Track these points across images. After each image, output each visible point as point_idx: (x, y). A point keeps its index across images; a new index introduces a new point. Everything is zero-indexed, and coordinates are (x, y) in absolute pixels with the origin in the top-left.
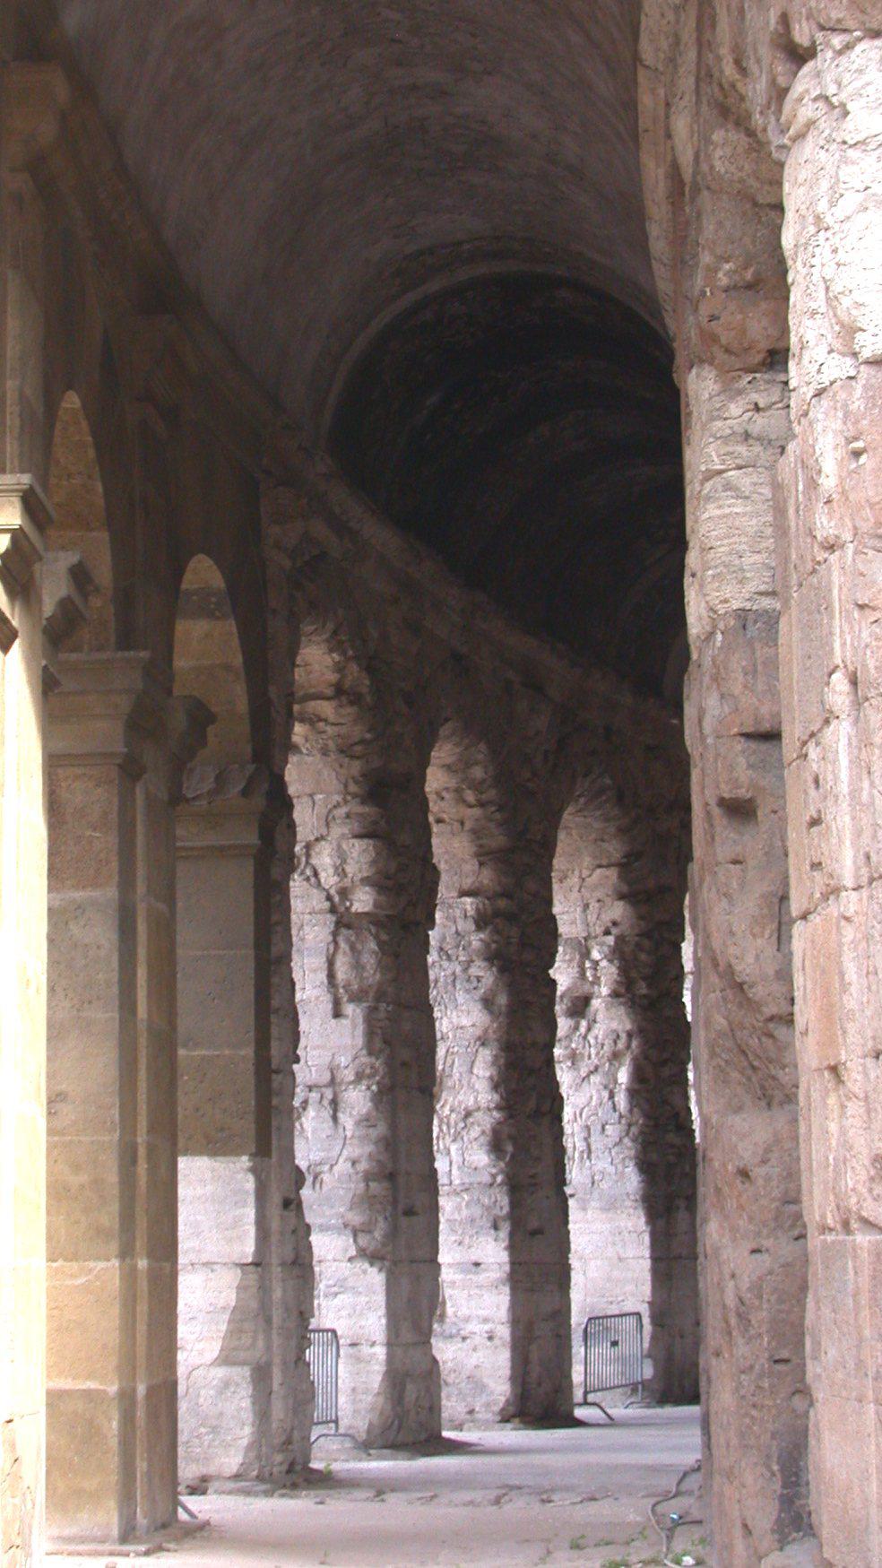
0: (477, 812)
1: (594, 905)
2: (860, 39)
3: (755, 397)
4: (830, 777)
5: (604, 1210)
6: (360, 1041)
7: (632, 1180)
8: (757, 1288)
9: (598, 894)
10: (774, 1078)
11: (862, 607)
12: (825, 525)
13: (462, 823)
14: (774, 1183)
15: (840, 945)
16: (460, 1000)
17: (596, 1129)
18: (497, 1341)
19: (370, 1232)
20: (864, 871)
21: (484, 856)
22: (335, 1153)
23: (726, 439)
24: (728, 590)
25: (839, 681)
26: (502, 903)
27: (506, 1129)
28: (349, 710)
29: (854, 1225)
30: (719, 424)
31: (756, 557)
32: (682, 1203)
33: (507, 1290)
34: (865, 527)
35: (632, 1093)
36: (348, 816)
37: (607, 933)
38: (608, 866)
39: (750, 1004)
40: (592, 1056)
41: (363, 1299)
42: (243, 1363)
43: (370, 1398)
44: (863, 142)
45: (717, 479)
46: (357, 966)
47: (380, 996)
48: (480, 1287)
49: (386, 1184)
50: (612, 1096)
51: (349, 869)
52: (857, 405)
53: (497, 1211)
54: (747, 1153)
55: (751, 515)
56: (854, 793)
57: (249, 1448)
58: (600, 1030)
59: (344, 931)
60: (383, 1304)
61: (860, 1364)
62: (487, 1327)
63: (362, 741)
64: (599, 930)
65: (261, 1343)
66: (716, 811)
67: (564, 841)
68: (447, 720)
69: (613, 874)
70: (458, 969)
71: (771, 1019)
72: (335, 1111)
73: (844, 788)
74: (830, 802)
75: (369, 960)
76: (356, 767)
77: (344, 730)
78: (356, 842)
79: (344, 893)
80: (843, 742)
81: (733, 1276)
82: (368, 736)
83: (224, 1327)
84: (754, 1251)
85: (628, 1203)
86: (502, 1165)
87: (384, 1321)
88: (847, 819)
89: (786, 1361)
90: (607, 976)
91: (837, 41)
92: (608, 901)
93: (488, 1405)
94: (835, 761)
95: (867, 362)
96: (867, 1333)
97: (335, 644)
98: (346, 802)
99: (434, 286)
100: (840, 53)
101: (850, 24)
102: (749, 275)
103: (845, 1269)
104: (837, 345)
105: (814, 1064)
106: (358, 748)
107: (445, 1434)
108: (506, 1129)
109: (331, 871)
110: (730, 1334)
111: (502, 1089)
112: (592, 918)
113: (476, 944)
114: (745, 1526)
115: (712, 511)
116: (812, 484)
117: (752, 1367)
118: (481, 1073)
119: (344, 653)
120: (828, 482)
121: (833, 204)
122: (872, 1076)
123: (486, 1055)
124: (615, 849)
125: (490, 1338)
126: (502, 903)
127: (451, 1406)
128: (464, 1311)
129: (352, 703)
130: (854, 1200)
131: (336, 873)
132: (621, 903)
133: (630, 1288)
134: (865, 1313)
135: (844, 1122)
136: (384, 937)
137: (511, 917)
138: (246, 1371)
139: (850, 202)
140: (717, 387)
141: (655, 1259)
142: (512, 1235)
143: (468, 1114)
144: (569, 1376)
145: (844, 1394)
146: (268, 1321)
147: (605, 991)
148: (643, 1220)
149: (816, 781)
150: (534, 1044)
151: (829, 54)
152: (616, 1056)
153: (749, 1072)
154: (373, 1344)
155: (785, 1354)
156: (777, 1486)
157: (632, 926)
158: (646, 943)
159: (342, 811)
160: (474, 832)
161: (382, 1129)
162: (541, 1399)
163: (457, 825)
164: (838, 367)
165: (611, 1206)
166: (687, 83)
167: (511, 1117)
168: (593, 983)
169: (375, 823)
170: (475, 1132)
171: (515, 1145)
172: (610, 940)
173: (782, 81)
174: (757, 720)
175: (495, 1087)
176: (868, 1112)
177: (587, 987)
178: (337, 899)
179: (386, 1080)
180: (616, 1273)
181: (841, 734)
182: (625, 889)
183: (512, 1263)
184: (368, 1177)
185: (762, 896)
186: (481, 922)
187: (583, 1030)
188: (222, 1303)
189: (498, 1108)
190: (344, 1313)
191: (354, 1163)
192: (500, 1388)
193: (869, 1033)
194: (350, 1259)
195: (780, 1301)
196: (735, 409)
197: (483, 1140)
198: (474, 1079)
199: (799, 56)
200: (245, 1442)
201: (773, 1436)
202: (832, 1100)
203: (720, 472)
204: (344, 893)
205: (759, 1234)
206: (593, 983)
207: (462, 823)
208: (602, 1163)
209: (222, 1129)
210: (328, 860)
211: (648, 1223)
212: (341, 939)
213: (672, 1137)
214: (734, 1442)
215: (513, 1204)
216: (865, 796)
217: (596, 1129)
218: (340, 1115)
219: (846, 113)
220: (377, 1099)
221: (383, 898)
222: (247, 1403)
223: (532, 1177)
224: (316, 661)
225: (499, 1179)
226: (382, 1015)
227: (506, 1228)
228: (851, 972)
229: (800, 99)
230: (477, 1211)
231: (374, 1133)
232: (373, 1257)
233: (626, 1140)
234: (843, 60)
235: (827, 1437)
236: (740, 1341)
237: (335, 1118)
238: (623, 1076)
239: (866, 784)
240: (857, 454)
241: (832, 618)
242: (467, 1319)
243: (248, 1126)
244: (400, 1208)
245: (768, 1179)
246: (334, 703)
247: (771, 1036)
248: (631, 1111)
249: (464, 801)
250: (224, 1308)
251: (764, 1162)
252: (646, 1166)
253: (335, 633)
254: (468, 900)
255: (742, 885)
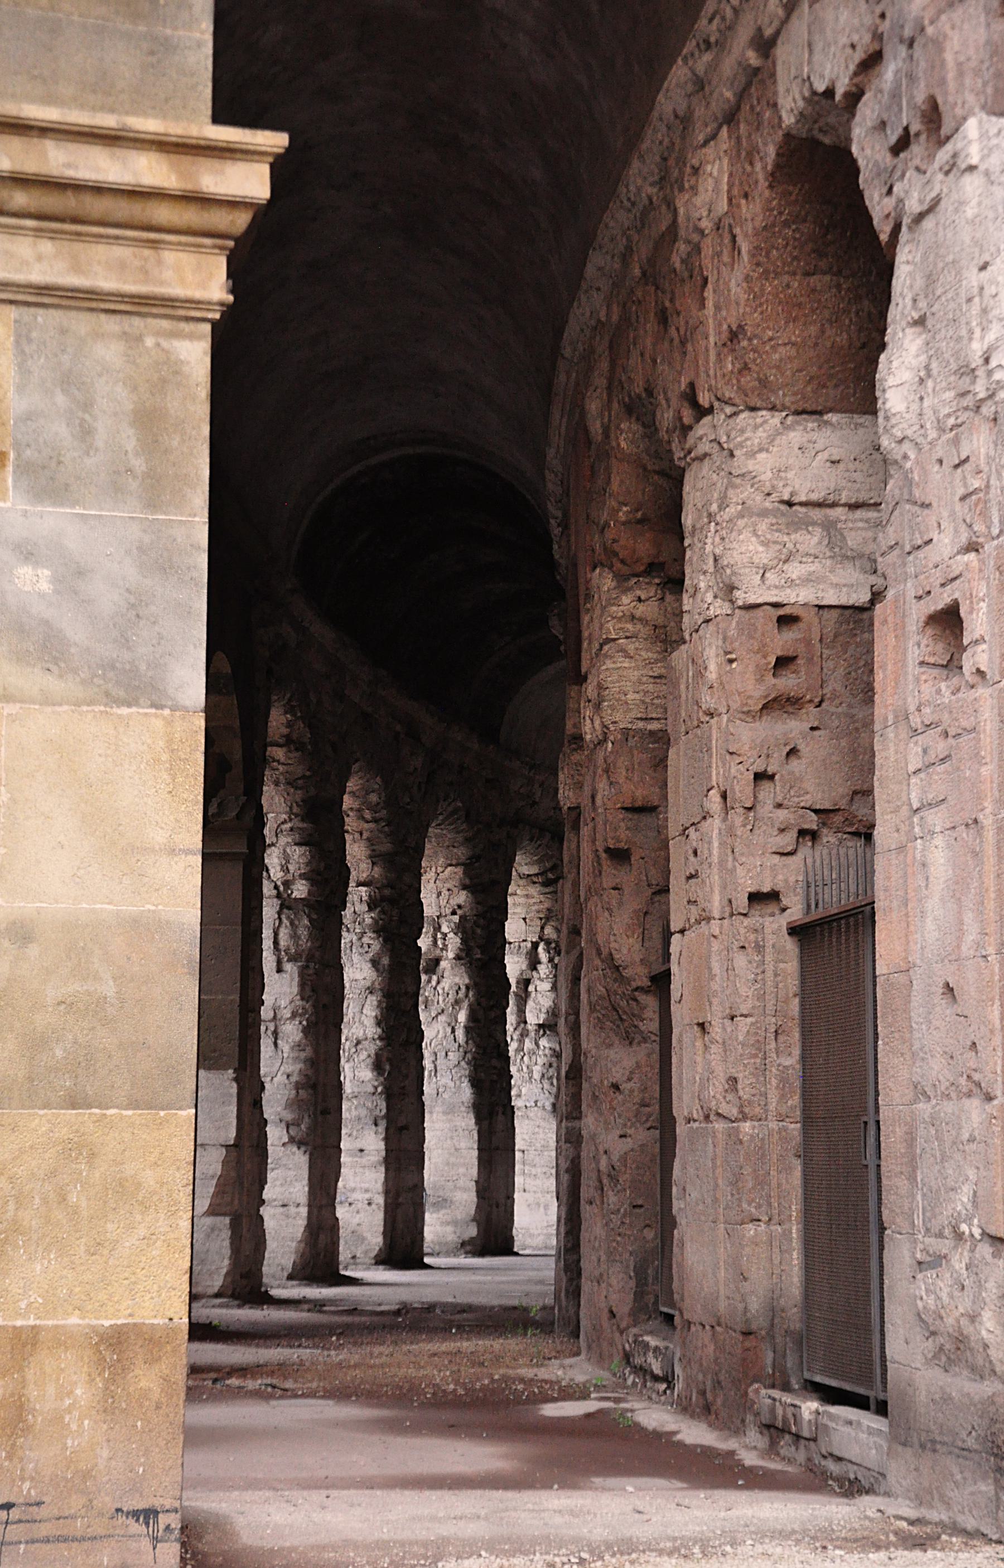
0: (372, 825)
1: (445, 892)
2: (742, 411)
3: (638, 593)
4: (706, 852)
5: (445, 1113)
6: (295, 990)
7: (466, 1092)
8: (624, 1159)
9: (448, 885)
10: (636, 1027)
11: (731, 753)
12: (708, 701)
13: (361, 834)
14: (636, 1093)
15: (710, 951)
16: (355, 960)
17: (441, 1055)
18: (374, 1206)
19: (299, 1125)
20: (728, 909)
21: (375, 858)
22: (275, 1069)
23: (620, 619)
24: (618, 716)
25: (715, 795)
26: (387, 892)
27: (385, 1054)
28: (298, 754)
29: (712, 1117)
30: (615, 608)
31: (637, 696)
32: (500, 1110)
33: (383, 1169)
34: (734, 706)
35: (468, 1029)
36: (292, 829)
37: (454, 913)
38: (456, 865)
39: (621, 979)
40: (441, 1002)
41: (292, 1173)
42: (224, 1214)
43: (294, 1244)
44: (743, 475)
45: (612, 644)
46: (294, 936)
47: (310, 958)
48: (364, 1167)
49: (310, 1091)
50: (453, 1031)
51: (291, 868)
52: (732, 632)
53: (377, 1112)
54: (617, 1075)
55: (634, 668)
56: (722, 863)
57: (227, 1274)
58: (446, 984)
59: (285, 911)
60: (307, 1177)
61: (716, 1200)
62: (367, 1196)
63: (304, 777)
64: (448, 911)
65: (236, 1202)
66: (604, 855)
67: (428, 848)
68: (357, 761)
69: (460, 870)
70: (355, 938)
71: (637, 989)
72: (276, 1039)
73: (715, 859)
74: (705, 866)
75: (303, 933)
76: (299, 795)
77: (291, 769)
78: (297, 848)
79: (287, 884)
80: (716, 831)
81: (606, 1152)
82: (308, 773)
83: (212, 1190)
84: (621, 1136)
85: (463, 1109)
86: (382, 1079)
87: (307, 1189)
88: (716, 877)
89: (641, 1206)
90: (454, 942)
91: (729, 410)
92: (455, 890)
93: (366, 1252)
94: (710, 843)
95: (740, 608)
96: (720, 1182)
97: (289, 709)
98: (291, 820)
99: (373, 461)
100: (730, 417)
101: (737, 401)
102: (639, 515)
103: (705, 1144)
104: (721, 594)
105: (687, 1021)
106: (300, 782)
107: (342, 1272)
108: (385, 1054)
109: (279, 868)
110: (602, 1190)
111: (383, 1025)
112: (443, 902)
113: (368, 921)
114: (611, 1312)
115: (609, 664)
116: (700, 673)
117: (619, 1210)
118: (369, 1013)
119: (294, 715)
120: (712, 673)
121: (721, 508)
122: (729, 1030)
123: (373, 1000)
124: (461, 853)
125: (369, 1204)
126: (387, 892)
127: (344, 1254)
128: (351, 1184)
129: (297, 750)
130: (714, 1103)
131: (282, 870)
132: (465, 892)
133: (462, 1170)
134: (719, 1170)
135: (708, 1056)
136: (315, 917)
137: (392, 901)
138: (227, 1220)
139: (732, 510)
140: (614, 584)
141: (480, 1149)
142: (387, 1129)
143: (358, 1043)
144: (422, 1232)
145: (703, 1218)
146: (242, 1184)
147: (451, 955)
148: (473, 1121)
149: (695, 853)
150: (406, 993)
151: (723, 417)
152: (457, 1002)
153: (619, 1022)
154: (298, 1205)
155: (640, 1202)
156: (632, 1284)
157: (472, 909)
158: (482, 921)
159: (288, 825)
160: (368, 839)
161: (309, 1052)
162: (403, 1249)
163: (357, 836)
164: (719, 608)
165: (450, 1110)
166: (600, 381)
167: (389, 1045)
168: (442, 950)
169: (310, 835)
170: (364, 1055)
171: (391, 1065)
172: (456, 918)
173: (686, 421)
174: (634, 800)
175: (378, 1024)
176: (725, 1051)
177: (438, 952)
178: (282, 888)
179: (313, 1018)
180: (452, 1160)
181: (714, 826)
182: (467, 881)
183: (387, 1150)
184: (298, 1086)
185: (635, 911)
186: (372, 905)
187: (434, 983)
188: (211, 1172)
189: (380, 1038)
190: (278, 1183)
191: (288, 1076)
192: (375, 1240)
193: (727, 1005)
194: (284, 1145)
195: (638, 1168)
196: (625, 600)
197: (369, 1061)
198: (363, 1017)
199: (702, 412)
200: (225, 1270)
201: (631, 1254)
202: (699, 1044)
203: (615, 640)
204: (287, 884)
205: (625, 1125)
206: (442, 950)
207: (361, 834)
208: (445, 1079)
209: (215, 1051)
210: (276, 861)
211: (476, 1123)
212: (283, 917)
213: (495, 1062)
214: (603, 1258)
215: (388, 1108)
216: (730, 865)
217: (441, 1055)
218: (279, 1042)
219: (732, 455)
220: (306, 1031)
221: (315, 888)
222: (227, 1243)
223: (403, 1088)
224: (278, 721)
225: (380, 1089)
226: (311, 972)
227: (383, 1125)
228: (716, 967)
229: (701, 438)
230: (363, 1112)
231: (303, 1055)
232: (300, 1143)
233: (463, 1063)
234: (731, 421)
235: (689, 1247)
236: (610, 1193)
237: (276, 1044)
238: (462, 1017)
239: (730, 859)
240: (731, 661)
241: (711, 757)
242: (353, 1190)
243: (234, 1047)
244: (319, 1108)
245: (632, 1091)
246: (284, 749)
247: (635, 1000)
248: (467, 1043)
249: (363, 818)
250: (213, 1177)
251: (629, 1079)
252: (475, 1083)
253: (290, 700)
254: (364, 889)
255: (620, 904)
